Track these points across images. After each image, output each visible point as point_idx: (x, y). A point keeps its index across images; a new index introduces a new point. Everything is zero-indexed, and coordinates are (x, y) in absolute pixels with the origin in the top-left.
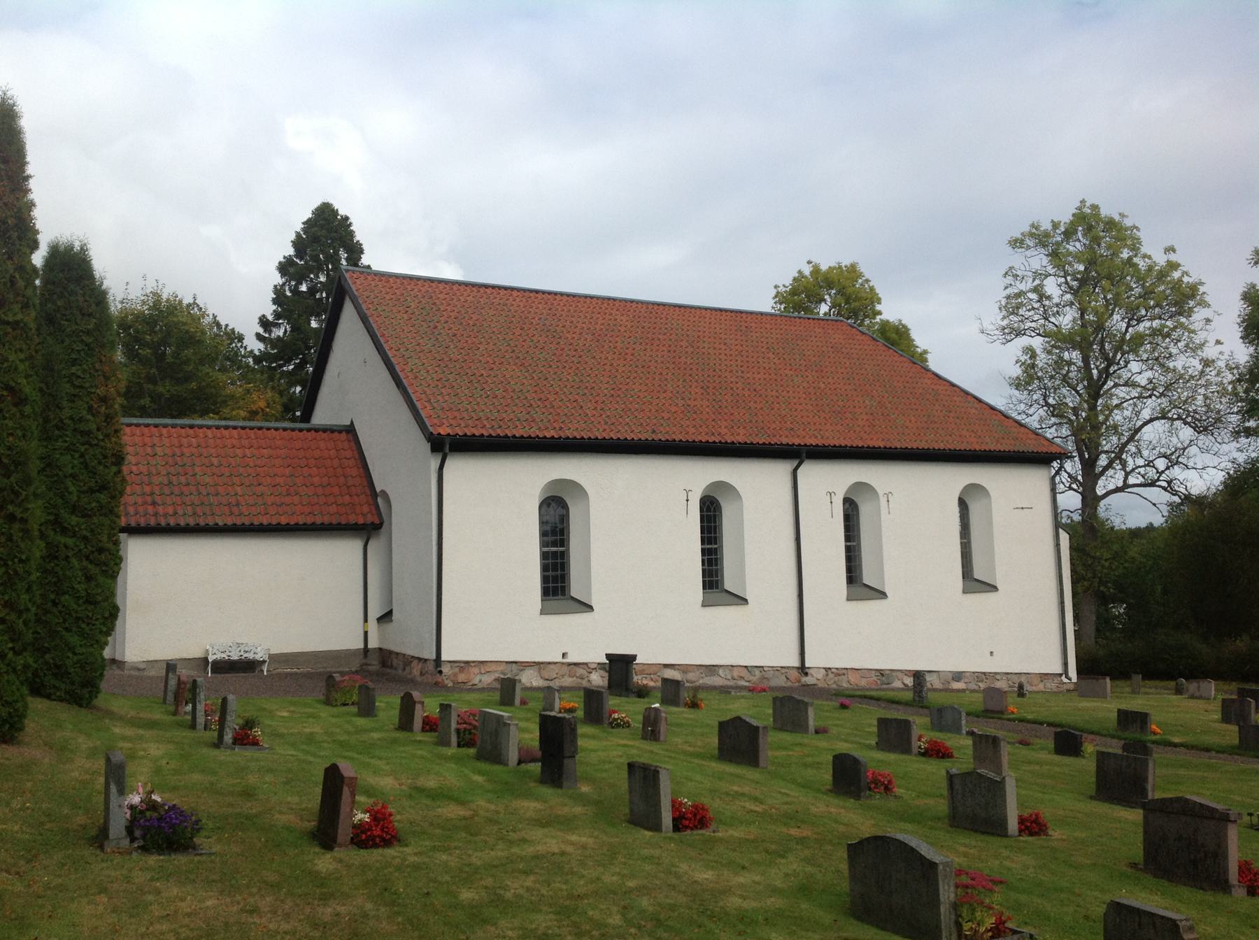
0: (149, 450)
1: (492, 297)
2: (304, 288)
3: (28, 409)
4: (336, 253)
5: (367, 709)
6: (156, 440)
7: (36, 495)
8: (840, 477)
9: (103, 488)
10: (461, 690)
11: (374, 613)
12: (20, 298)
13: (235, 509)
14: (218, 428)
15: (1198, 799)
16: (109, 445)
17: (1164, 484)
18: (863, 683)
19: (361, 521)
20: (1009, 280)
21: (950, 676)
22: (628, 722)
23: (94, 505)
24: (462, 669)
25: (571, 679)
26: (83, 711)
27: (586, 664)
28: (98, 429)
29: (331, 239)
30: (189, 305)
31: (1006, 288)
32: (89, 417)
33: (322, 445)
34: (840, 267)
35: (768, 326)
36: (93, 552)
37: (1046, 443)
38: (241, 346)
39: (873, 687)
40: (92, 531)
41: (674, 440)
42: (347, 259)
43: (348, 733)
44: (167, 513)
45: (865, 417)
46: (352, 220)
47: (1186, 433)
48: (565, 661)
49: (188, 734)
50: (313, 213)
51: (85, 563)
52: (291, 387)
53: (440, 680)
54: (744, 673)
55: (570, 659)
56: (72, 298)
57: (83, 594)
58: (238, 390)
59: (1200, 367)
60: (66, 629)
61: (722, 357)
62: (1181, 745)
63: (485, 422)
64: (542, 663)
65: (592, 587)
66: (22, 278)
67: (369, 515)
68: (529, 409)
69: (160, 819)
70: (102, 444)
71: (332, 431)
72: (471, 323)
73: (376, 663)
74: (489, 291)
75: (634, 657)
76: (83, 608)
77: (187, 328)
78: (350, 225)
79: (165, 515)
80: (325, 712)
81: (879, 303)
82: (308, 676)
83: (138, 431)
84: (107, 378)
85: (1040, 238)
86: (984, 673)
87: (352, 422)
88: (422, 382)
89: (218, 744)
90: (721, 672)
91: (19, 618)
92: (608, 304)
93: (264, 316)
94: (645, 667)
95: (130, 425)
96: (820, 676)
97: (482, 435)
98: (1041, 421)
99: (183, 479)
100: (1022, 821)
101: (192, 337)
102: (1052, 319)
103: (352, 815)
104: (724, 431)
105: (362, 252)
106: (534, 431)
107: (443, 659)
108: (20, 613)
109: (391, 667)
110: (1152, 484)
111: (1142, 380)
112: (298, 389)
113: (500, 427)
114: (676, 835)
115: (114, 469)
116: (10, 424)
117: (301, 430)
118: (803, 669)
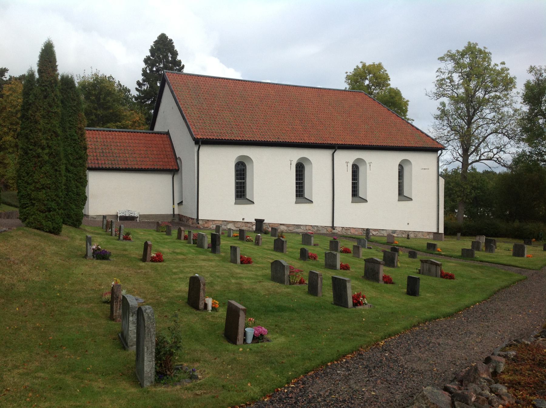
0: (95, 140)
1: (221, 82)
2: (154, 69)
3: (59, 138)
4: (167, 55)
5: (169, 233)
6: (97, 136)
7: (63, 164)
8: (350, 157)
9: (81, 158)
10: (205, 229)
11: (176, 202)
12: (56, 104)
13: (126, 163)
14: (119, 132)
15: (376, 259)
16: (82, 144)
17: (496, 159)
18: (356, 233)
19: (171, 168)
20: (438, 74)
21: (391, 231)
22: (252, 240)
23: (78, 163)
24: (206, 223)
25: (246, 228)
26: (77, 229)
27: (251, 222)
28: (79, 139)
29: (165, 49)
30: (109, 77)
31: (437, 77)
32: (76, 135)
33: (157, 139)
34: (374, 65)
35: (331, 95)
36: (78, 179)
37: (436, 143)
38: (129, 94)
39: (360, 234)
40: (78, 172)
41: (286, 142)
42: (171, 57)
43: (160, 239)
44: (102, 163)
45: (364, 133)
46: (173, 41)
47: (506, 139)
48: (243, 221)
49: (111, 237)
50: (158, 38)
51: (76, 182)
52: (149, 110)
53: (198, 226)
54: (310, 228)
55: (245, 221)
56: (69, 95)
57: (76, 192)
58: (129, 113)
59: (512, 112)
60: (71, 203)
61: (310, 108)
62: (444, 255)
63: (215, 134)
64: (236, 222)
65: (254, 195)
66: (56, 98)
67: (174, 166)
68: (232, 129)
69: (100, 252)
70: (80, 143)
71: (161, 134)
72: (212, 93)
73: (177, 219)
74: (220, 80)
75: (263, 220)
76: (76, 196)
77: (108, 88)
78: (173, 43)
79: (102, 164)
80: (155, 233)
81: (390, 81)
82: (152, 222)
83: (91, 132)
84: (81, 122)
85: (452, 57)
86: (405, 231)
87: (168, 131)
88: (192, 118)
89: (119, 239)
90: (302, 227)
91: (60, 199)
92: (267, 86)
93: (139, 81)
94: (273, 225)
95: (88, 130)
96: (340, 230)
97: (213, 139)
98: (448, 132)
99: (107, 151)
100: (341, 265)
101: (110, 92)
102: (455, 91)
103: (150, 254)
104: (305, 138)
105: (177, 54)
106: (233, 138)
107: (199, 219)
108: (60, 198)
109: (183, 221)
110: (491, 159)
111: (490, 116)
112: (152, 111)
113: (220, 136)
114: (241, 265)
115: (84, 152)
116: (55, 142)
117: (150, 133)
118: (333, 227)
